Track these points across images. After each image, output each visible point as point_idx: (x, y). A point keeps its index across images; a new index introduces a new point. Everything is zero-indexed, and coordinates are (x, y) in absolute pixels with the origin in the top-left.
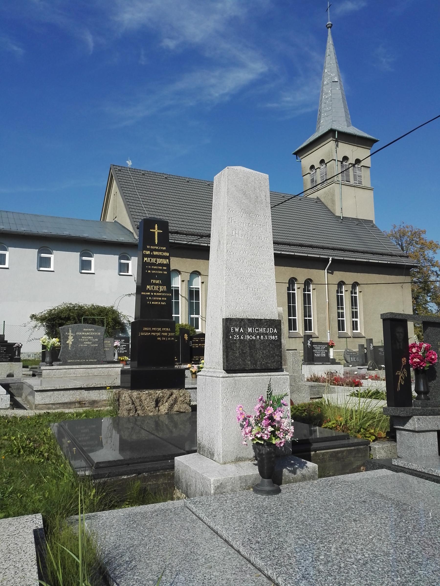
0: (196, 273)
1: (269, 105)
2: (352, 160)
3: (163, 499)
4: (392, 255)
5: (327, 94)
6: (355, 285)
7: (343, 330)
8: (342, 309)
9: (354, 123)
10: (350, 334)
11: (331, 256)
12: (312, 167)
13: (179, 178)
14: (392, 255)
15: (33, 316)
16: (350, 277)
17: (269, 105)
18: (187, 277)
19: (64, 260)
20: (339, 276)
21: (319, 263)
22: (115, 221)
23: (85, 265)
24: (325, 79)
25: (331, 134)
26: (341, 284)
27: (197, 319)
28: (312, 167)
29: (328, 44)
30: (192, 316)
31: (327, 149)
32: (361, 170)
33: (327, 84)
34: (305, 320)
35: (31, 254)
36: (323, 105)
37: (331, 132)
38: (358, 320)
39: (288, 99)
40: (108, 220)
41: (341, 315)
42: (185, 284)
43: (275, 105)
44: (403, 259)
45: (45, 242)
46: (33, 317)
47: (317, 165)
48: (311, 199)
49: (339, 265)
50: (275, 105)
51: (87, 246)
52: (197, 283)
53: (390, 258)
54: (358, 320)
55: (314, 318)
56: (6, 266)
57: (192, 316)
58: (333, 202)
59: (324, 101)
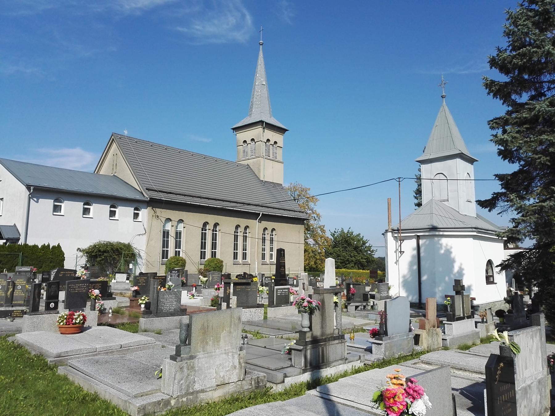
0: (181, 221)
1: (179, 29)
2: (272, 142)
3: (107, 408)
4: (295, 211)
5: (258, 92)
6: (273, 230)
7: (237, 259)
8: (265, 245)
9: (273, 114)
10: (268, 262)
11: (262, 211)
12: (245, 142)
13: (159, 145)
14: (295, 211)
15: (79, 249)
16: (270, 225)
17: (179, 29)
18: (175, 224)
19: (99, 210)
20: (265, 224)
21: (253, 216)
22: (114, 175)
23: (112, 214)
24: (257, 81)
25: (261, 123)
26: (265, 229)
27: (179, 251)
28: (245, 142)
29: (260, 57)
30: (176, 250)
31: (257, 132)
32: (276, 149)
33: (258, 85)
34: (212, 252)
35: (79, 206)
36: (255, 100)
37: (261, 122)
38: (273, 253)
39: (198, 27)
40: (101, 173)
41: (264, 250)
42: (174, 228)
43: (185, 30)
44: (301, 214)
45: (88, 198)
46: (461, 264)
47: (249, 141)
48: (244, 165)
49: (267, 217)
50: (185, 30)
51: (114, 201)
52: (181, 227)
53: (293, 213)
54: (273, 253)
55: (248, 252)
56: (62, 213)
57: (176, 250)
58: (259, 170)
59: (255, 96)
